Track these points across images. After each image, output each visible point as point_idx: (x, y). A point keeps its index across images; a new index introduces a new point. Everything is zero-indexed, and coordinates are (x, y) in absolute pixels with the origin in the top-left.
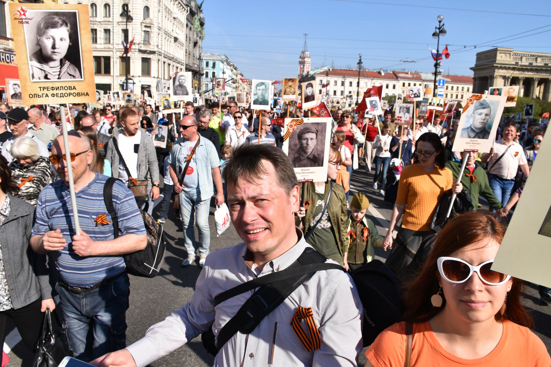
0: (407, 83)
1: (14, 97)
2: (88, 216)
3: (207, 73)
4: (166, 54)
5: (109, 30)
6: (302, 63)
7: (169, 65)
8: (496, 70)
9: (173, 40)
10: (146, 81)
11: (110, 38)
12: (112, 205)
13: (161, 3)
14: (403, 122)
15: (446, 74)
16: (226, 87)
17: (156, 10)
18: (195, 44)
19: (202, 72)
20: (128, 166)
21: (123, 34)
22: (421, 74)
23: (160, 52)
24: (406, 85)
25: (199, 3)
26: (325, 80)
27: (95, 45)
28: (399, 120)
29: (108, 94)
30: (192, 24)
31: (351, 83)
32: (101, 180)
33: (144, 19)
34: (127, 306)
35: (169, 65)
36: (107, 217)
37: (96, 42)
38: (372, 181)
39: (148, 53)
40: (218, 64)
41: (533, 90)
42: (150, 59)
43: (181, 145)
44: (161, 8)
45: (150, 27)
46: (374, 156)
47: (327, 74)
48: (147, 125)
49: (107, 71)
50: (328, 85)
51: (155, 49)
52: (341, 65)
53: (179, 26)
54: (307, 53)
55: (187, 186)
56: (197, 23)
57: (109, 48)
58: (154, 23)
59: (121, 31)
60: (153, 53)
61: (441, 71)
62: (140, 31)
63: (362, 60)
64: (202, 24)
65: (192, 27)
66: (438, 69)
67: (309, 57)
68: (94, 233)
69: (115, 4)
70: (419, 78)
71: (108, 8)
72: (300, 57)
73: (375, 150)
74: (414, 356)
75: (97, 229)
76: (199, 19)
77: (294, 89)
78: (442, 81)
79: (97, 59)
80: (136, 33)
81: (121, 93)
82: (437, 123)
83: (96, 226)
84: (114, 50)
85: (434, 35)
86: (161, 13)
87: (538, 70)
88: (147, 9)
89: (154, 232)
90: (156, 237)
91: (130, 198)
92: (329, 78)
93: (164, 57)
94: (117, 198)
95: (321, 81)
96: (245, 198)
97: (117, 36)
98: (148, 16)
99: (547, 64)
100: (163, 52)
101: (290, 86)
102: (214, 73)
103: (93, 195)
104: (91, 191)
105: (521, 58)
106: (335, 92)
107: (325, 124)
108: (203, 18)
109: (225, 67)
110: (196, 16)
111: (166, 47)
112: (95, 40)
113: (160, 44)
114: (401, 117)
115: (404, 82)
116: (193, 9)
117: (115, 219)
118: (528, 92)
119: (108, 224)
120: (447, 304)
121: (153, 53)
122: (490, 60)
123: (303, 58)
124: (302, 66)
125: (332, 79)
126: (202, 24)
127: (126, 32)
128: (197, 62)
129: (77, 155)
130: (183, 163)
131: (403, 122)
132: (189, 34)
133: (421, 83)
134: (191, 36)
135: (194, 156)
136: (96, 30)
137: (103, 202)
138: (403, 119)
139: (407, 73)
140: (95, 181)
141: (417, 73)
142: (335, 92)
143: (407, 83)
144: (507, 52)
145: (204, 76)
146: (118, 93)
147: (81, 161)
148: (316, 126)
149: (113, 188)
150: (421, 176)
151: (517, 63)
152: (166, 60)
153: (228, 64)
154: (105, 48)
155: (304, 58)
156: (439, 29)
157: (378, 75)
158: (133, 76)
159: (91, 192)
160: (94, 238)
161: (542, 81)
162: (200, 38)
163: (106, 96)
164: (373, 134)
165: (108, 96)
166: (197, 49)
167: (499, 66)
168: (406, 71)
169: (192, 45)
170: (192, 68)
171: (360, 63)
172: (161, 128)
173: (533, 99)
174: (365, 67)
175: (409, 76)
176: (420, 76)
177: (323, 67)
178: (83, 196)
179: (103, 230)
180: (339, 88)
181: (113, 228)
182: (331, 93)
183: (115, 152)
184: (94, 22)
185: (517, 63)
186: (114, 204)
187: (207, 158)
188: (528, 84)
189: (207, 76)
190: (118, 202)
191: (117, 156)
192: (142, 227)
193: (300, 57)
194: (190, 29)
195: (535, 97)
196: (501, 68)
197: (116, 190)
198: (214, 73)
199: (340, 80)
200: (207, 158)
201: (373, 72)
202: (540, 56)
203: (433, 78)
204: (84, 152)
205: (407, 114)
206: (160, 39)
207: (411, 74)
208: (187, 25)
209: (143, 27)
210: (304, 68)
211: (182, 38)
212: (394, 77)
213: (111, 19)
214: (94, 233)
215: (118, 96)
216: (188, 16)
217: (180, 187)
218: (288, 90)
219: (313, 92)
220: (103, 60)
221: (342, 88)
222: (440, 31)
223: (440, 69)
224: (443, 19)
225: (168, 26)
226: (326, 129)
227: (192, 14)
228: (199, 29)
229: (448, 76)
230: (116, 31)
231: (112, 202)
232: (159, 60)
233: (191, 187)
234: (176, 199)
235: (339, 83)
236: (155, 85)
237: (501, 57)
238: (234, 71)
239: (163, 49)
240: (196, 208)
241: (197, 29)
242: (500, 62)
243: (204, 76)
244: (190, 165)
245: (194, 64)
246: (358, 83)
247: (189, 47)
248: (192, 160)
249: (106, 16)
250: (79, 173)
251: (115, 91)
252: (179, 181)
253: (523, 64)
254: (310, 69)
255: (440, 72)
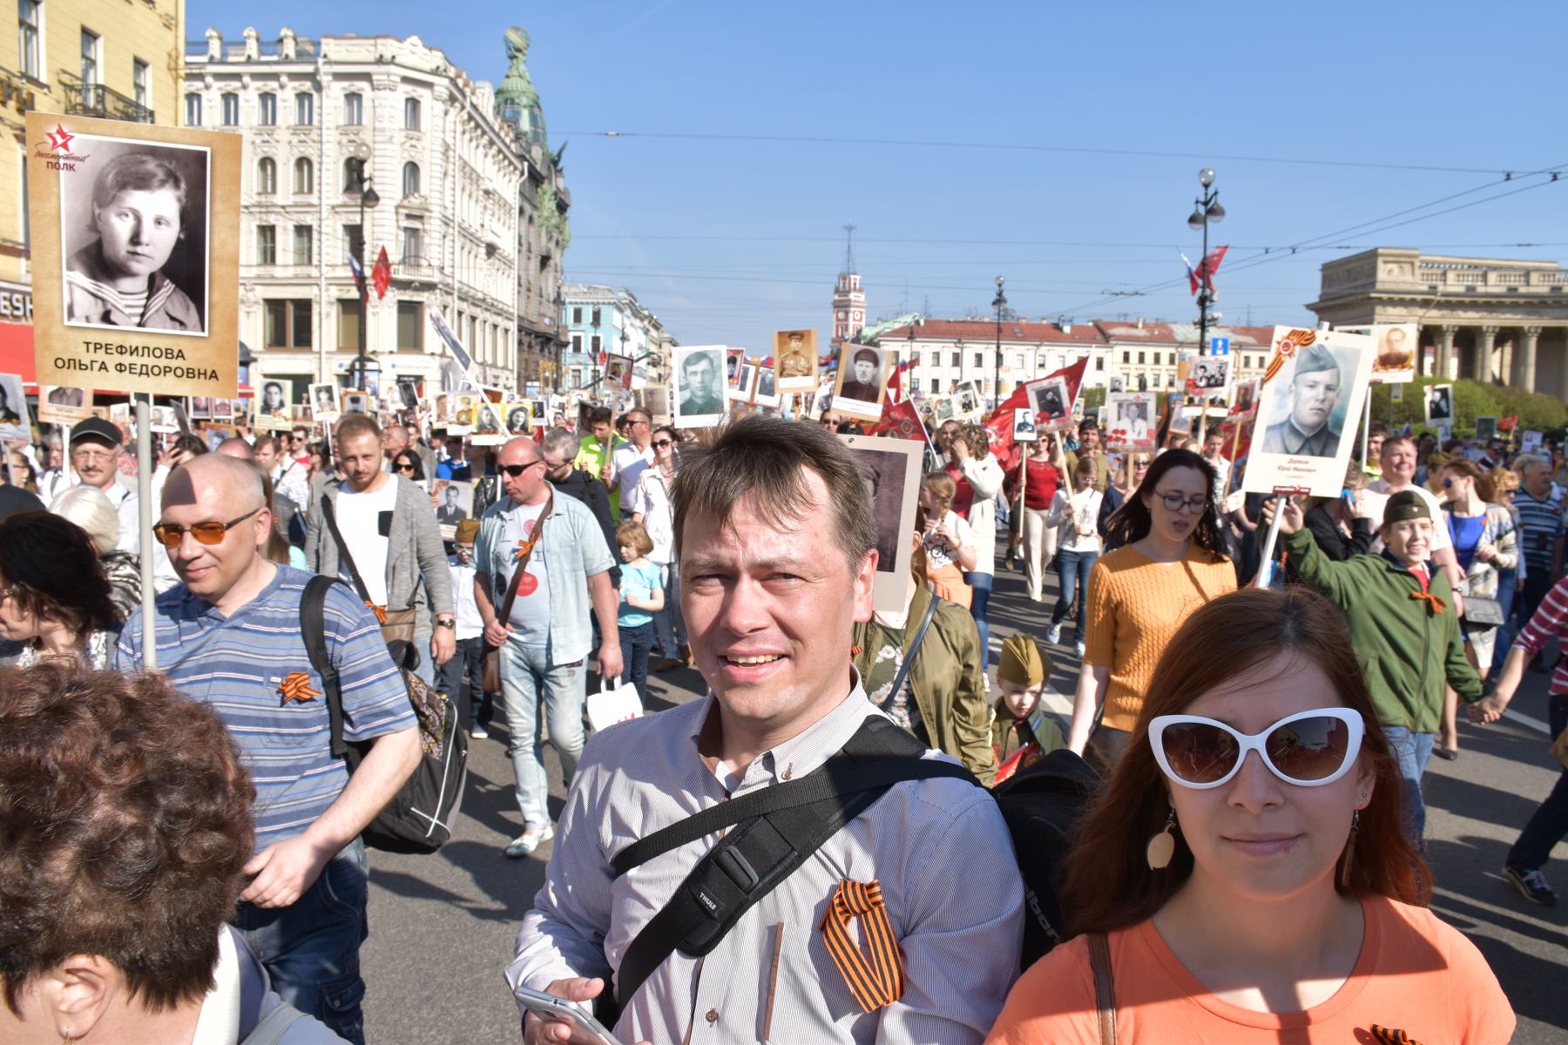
0: (1134, 352)
1: (56, 398)
2: (260, 679)
3: (577, 340)
4: (465, 289)
5: (309, 229)
6: (843, 306)
7: (474, 319)
8: (1378, 309)
9: (483, 250)
10: (411, 364)
11: (310, 249)
12: (324, 648)
13: (451, 153)
14: (1130, 443)
15: (1243, 324)
16: (634, 379)
17: (438, 171)
18: (545, 260)
19: (563, 339)
20: (361, 573)
21: (347, 238)
22: (1173, 327)
23: (447, 285)
24: (1134, 358)
25: (553, 149)
26: (905, 351)
27: (270, 270)
28: (1117, 439)
29: (305, 405)
30: (535, 207)
31: (979, 357)
32: (293, 582)
33: (405, 197)
34: (364, 933)
35: (474, 319)
36: (312, 680)
37: (273, 261)
38: (1048, 621)
39: (416, 289)
40: (613, 318)
41: (1483, 360)
42: (420, 303)
43: (502, 518)
44: (451, 166)
45: (421, 217)
46: (1052, 550)
47: (911, 333)
48: (409, 464)
49: (303, 339)
50: (914, 363)
51: (436, 278)
52: (950, 309)
53: (500, 213)
54: (855, 279)
55: (518, 626)
56: (549, 205)
57: (309, 277)
58: (432, 208)
59: (340, 230)
60: (429, 287)
61: (1216, 315)
62: (394, 230)
63: (1005, 295)
64: (562, 207)
65: (535, 214)
66: (1208, 312)
67: (861, 290)
68: (277, 722)
69: (325, 159)
70: (1166, 338)
71: (306, 168)
72: (837, 291)
73: (1054, 530)
74: (1125, 1028)
75: (283, 713)
76: (555, 194)
77: (808, 360)
78: (1220, 343)
79: (275, 307)
80: (383, 231)
81: (337, 391)
82: (1213, 451)
83: (283, 704)
84: (323, 282)
85: (1193, 220)
86: (450, 179)
87: (1490, 304)
88: (412, 168)
89: (433, 724)
90: (440, 737)
91: (371, 628)
92: (917, 346)
93: (460, 298)
94: (337, 628)
95: (897, 354)
96: (742, 565)
97: (330, 250)
98: (417, 189)
99: (1516, 289)
100: (457, 285)
101: (796, 353)
102: (596, 340)
103: (272, 622)
104: (267, 612)
105: (1444, 274)
106: (936, 383)
107: (901, 459)
108: (566, 191)
109: (627, 322)
110: (545, 186)
111: (465, 271)
112: (269, 256)
113: (447, 263)
114: (1123, 432)
115: (1127, 349)
116: (538, 167)
117: (333, 684)
118: (1468, 367)
119: (312, 699)
120: (1197, 869)
121: (429, 287)
122: (1358, 283)
123: (843, 291)
124: (841, 315)
125: (925, 349)
126: (562, 207)
127: (355, 235)
128: (551, 310)
129: (230, 525)
130: (509, 564)
131: (1130, 443)
132: (528, 232)
133: (1173, 350)
134: (532, 240)
135: (538, 544)
136: (272, 228)
137: (299, 641)
138: (1130, 437)
139: (1134, 326)
140: (276, 586)
141: (1161, 325)
142: (936, 383)
143: (1134, 352)
144: (1404, 260)
145: (570, 348)
146: (329, 390)
147: (239, 540)
148: (875, 461)
149: (326, 603)
150: (1143, 568)
151: (1433, 289)
152: (464, 306)
153: (636, 314)
154: (296, 277)
155: (846, 292)
156: (1206, 203)
157: (1052, 333)
158: (374, 352)
159: (267, 615)
160: (275, 738)
161: (1506, 336)
162: (557, 243)
163: (300, 407)
164: (1045, 490)
165: (305, 410)
166: (550, 274)
167: (1385, 296)
168: (1131, 320)
169: (535, 263)
170: (536, 328)
171: (999, 301)
172: (453, 488)
173: (1481, 383)
174: (1019, 313)
175: (1140, 332)
176: (1171, 331)
177: (899, 314)
178: (245, 625)
179: (299, 716)
180: (947, 374)
181: (326, 712)
182: (926, 387)
183: (327, 534)
184: (267, 208)
185: (1433, 289)
186: (329, 644)
187: (576, 548)
188: (1468, 341)
189: (577, 349)
190: (339, 638)
191: (332, 544)
192: (403, 707)
193: (837, 291)
194: (531, 220)
195: (1488, 379)
196: (1391, 302)
197: (334, 606)
198: (596, 340)
199: (947, 350)
200: (574, 549)
201: (1040, 326)
202: (1495, 268)
203: (1195, 334)
204: (248, 516)
205: (1140, 423)
206: (448, 250)
207: (1145, 326)
208: (521, 211)
209: (402, 217)
210: (846, 319)
211: (508, 244)
212: (1099, 337)
213: (314, 199)
214: (277, 722)
215: (331, 398)
216: (523, 184)
217: (502, 630)
218: (790, 363)
219: (874, 377)
220: (290, 309)
221: (955, 373)
222: (1209, 210)
223: (1214, 312)
224: (1214, 177)
225: (471, 213)
226: (904, 473)
227: (535, 178)
228: (554, 221)
229: (1247, 331)
230: (329, 230)
231: (322, 639)
232: (445, 307)
233: (532, 631)
234: (492, 664)
235: (947, 358)
236: (438, 375)
237: (1390, 271)
238: (653, 333)
239: (457, 277)
240: (548, 707)
241: (548, 219)
242: (1387, 287)
243: (570, 348)
244: (528, 569)
245: (543, 315)
246: (999, 356)
247: (527, 270)
248: (533, 556)
249: (300, 191)
250: (233, 572)
251: (325, 383)
252: (497, 615)
253: (1451, 289)
254: (863, 323)
255: (1214, 319)
